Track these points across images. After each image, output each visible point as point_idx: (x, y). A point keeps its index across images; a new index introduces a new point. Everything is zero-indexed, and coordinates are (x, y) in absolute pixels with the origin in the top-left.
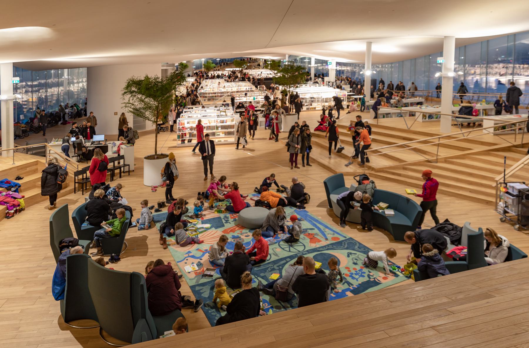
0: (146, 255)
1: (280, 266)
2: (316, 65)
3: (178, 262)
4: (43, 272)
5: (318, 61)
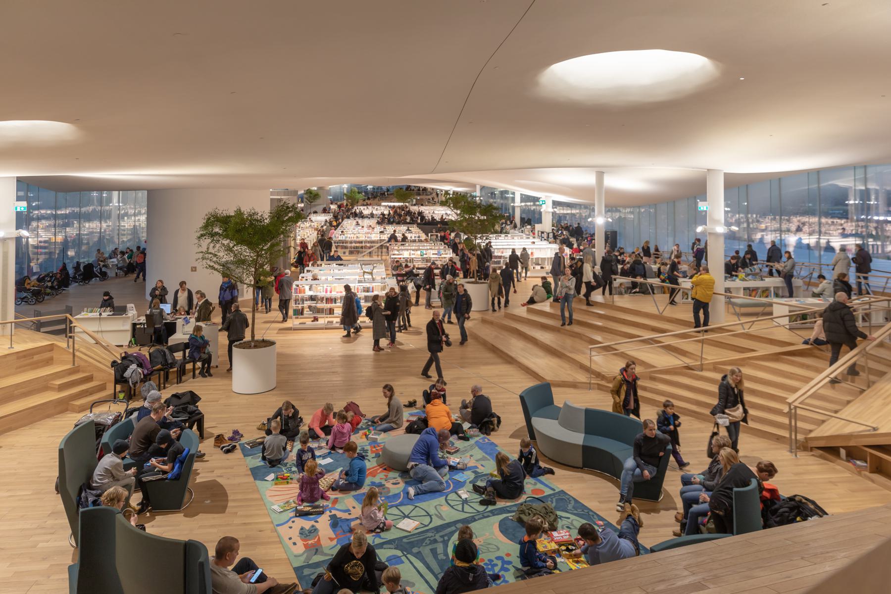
0: (224, 512)
1: (446, 535)
2: (523, 204)
3: (278, 525)
4: (49, 537)
5: (525, 198)
